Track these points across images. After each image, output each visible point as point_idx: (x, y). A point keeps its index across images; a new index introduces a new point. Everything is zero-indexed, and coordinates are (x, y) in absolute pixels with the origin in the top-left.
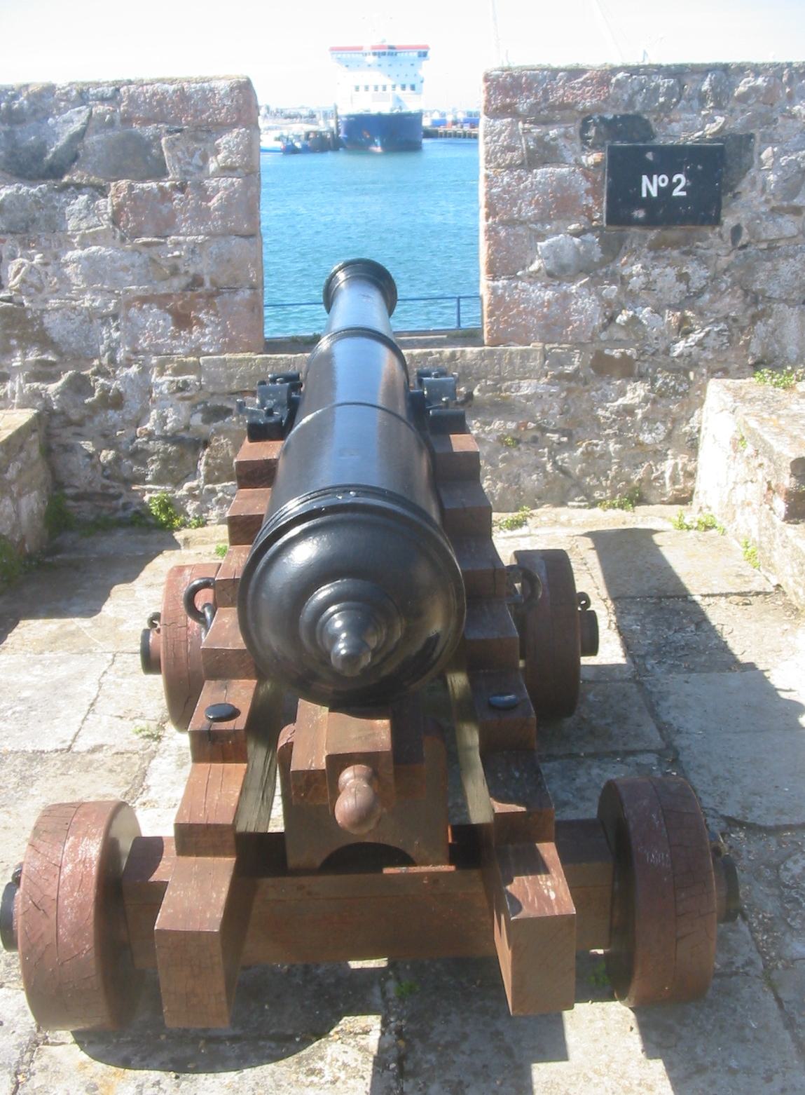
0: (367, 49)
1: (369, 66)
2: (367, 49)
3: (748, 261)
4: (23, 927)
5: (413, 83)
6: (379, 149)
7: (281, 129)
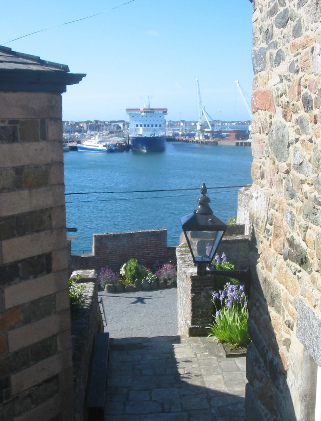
0: (142, 109)
1: (142, 116)
2: (142, 109)
3: (229, 220)
4: (313, 159)
5: (161, 124)
6: (145, 151)
7: (106, 142)
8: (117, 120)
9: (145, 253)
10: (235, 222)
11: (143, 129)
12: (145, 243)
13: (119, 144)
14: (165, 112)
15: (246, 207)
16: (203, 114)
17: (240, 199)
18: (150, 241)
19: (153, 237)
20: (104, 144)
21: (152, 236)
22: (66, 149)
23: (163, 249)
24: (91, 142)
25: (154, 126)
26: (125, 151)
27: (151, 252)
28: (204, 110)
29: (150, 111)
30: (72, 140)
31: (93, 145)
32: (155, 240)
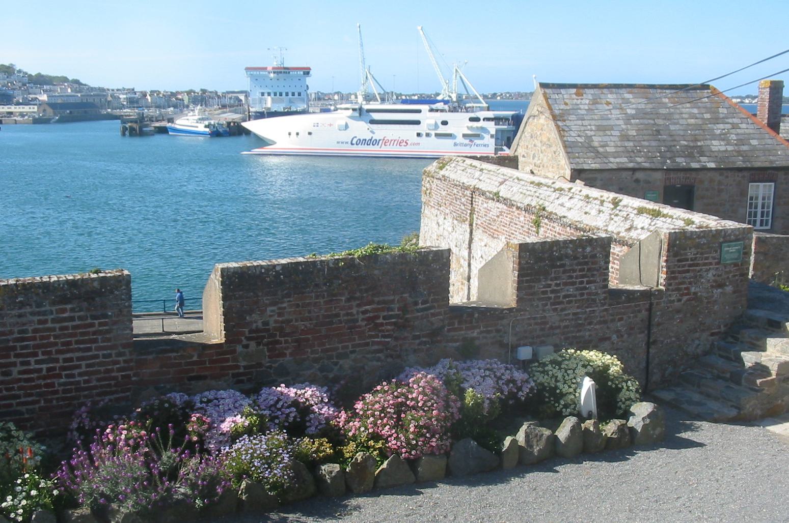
0: (270, 69)
1: (271, 80)
2: (270, 69)
8: (236, 90)
9: (41, 370)
10: (416, 244)
11: (272, 99)
12: (35, 331)
13: (234, 123)
14: (307, 72)
15: (441, 209)
16: (367, 78)
17: (427, 189)
18: (54, 321)
19: (69, 306)
20: (207, 123)
21: (64, 300)
22: (151, 131)
23: (120, 354)
24: (188, 119)
25: (290, 94)
26: (244, 135)
27: (63, 368)
28: (369, 72)
29: (283, 71)
30: (161, 119)
31: (190, 124)
32: (80, 318)
